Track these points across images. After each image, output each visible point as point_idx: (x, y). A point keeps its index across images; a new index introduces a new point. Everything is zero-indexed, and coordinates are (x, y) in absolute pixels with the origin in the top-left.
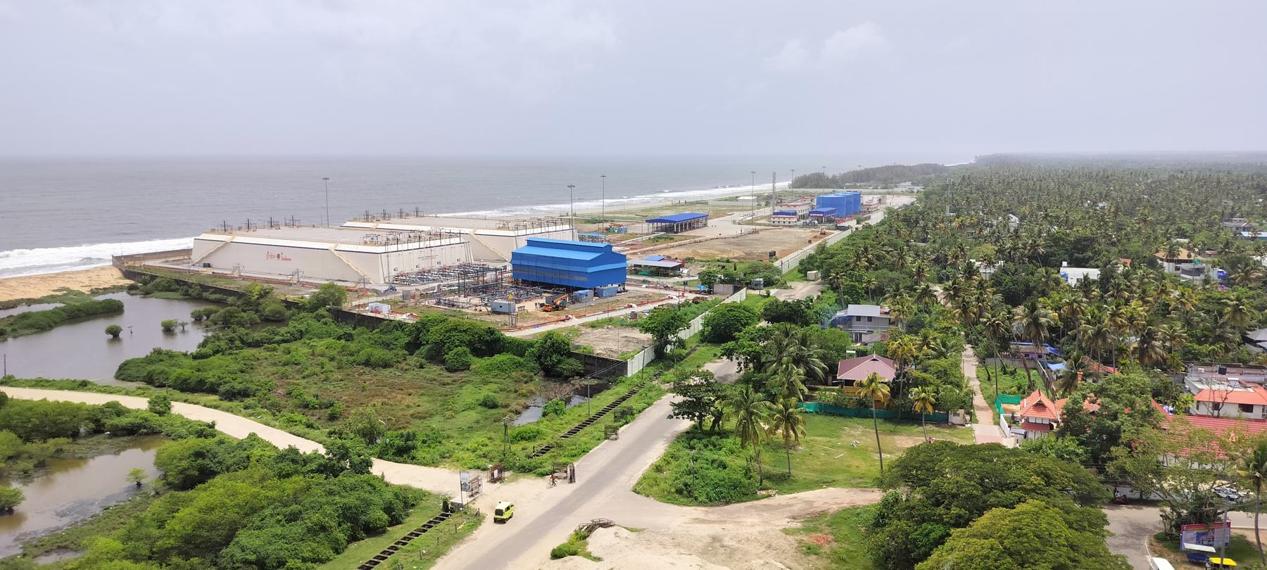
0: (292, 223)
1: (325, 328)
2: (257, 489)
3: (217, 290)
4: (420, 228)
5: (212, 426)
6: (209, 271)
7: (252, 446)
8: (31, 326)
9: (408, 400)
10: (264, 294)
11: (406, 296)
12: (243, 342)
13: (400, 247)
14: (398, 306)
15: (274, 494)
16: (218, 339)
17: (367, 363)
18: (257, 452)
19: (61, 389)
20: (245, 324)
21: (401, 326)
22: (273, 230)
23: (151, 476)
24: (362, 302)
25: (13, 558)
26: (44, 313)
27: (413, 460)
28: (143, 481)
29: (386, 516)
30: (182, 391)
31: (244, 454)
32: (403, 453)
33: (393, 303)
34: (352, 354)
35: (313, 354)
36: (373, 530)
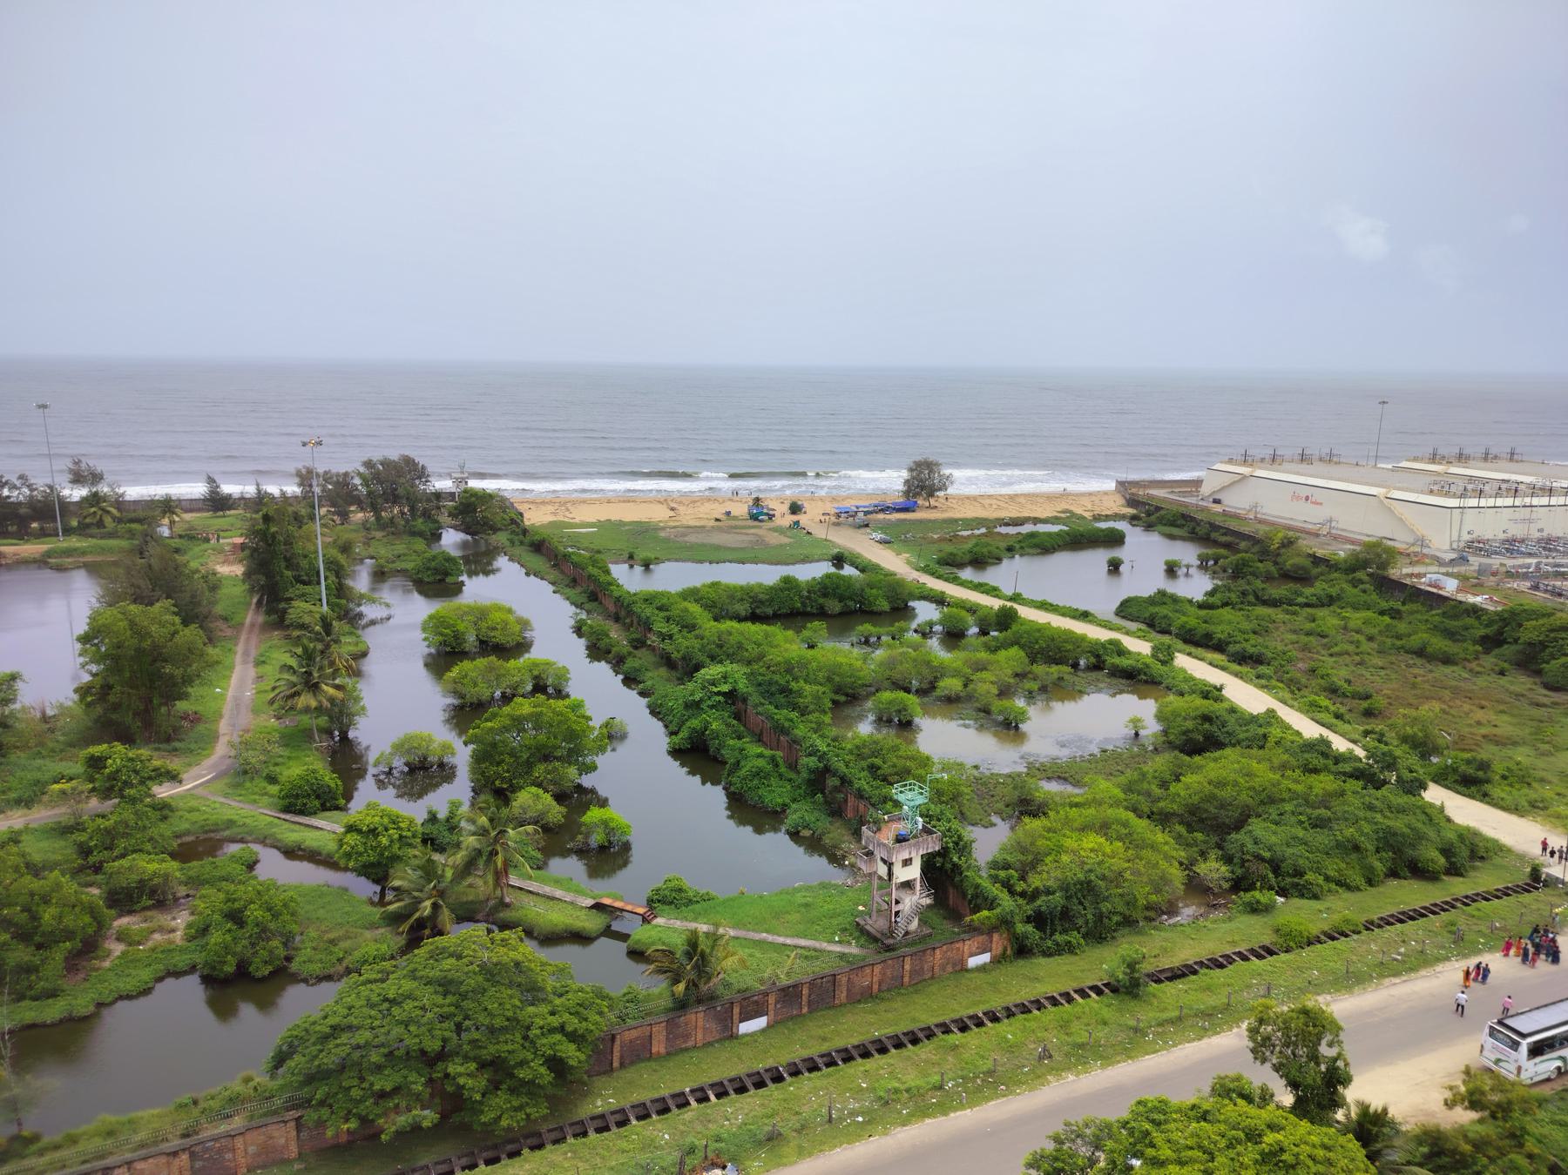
0: (1330, 459)
1: (1364, 597)
2: (1277, 777)
3: (1229, 532)
4: (1520, 478)
5: (1220, 689)
6: (1218, 508)
7: (1269, 724)
8: (1036, 546)
9: (1480, 715)
10: (1288, 543)
11: (1481, 571)
12: (1257, 597)
13: (1483, 502)
14: (1471, 583)
15: (1299, 788)
16: (1230, 590)
17: (1420, 653)
18: (1275, 732)
19: (1063, 615)
20: (1262, 579)
21: (1475, 611)
22: (1304, 466)
23: (1151, 728)
24: (1417, 570)
25: (1019, 775)
26: (1049, 534)
27: (1485, 797)
28: (1142, 732)
29: (1442, 860)
30: (1186, 641)
31: (1261, 731)
32: (1471, 782)
33: (1463, 578)
34: (1399, 637)
35: (1345, 628)
36: (1419, 871)
